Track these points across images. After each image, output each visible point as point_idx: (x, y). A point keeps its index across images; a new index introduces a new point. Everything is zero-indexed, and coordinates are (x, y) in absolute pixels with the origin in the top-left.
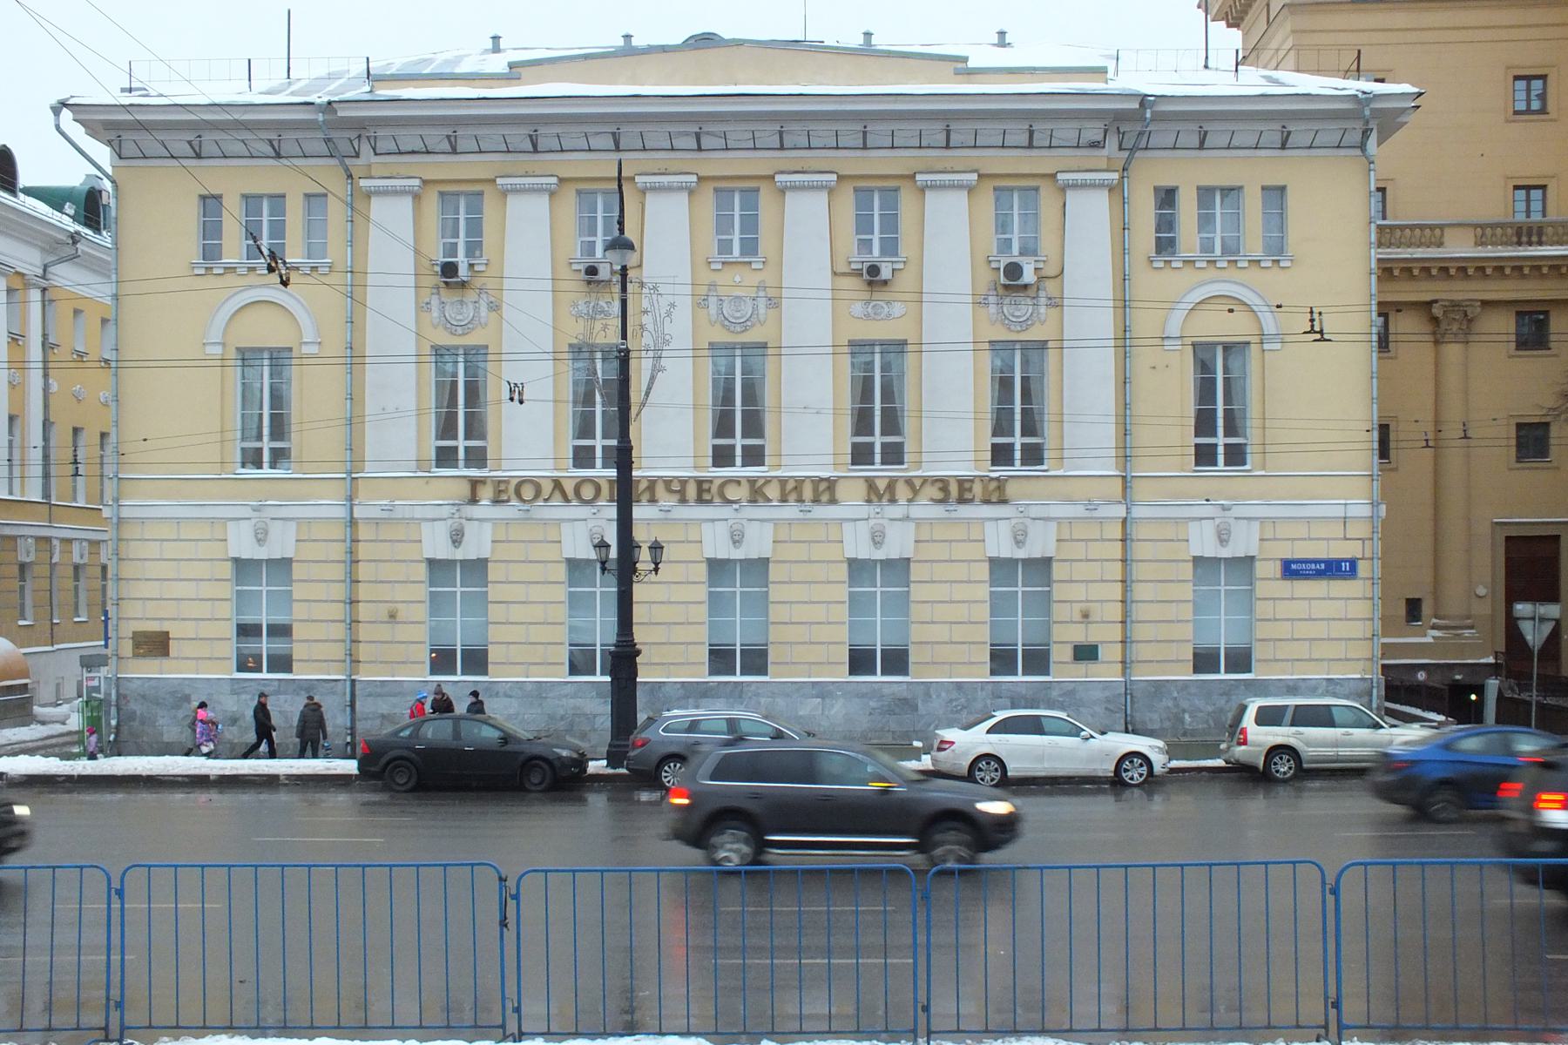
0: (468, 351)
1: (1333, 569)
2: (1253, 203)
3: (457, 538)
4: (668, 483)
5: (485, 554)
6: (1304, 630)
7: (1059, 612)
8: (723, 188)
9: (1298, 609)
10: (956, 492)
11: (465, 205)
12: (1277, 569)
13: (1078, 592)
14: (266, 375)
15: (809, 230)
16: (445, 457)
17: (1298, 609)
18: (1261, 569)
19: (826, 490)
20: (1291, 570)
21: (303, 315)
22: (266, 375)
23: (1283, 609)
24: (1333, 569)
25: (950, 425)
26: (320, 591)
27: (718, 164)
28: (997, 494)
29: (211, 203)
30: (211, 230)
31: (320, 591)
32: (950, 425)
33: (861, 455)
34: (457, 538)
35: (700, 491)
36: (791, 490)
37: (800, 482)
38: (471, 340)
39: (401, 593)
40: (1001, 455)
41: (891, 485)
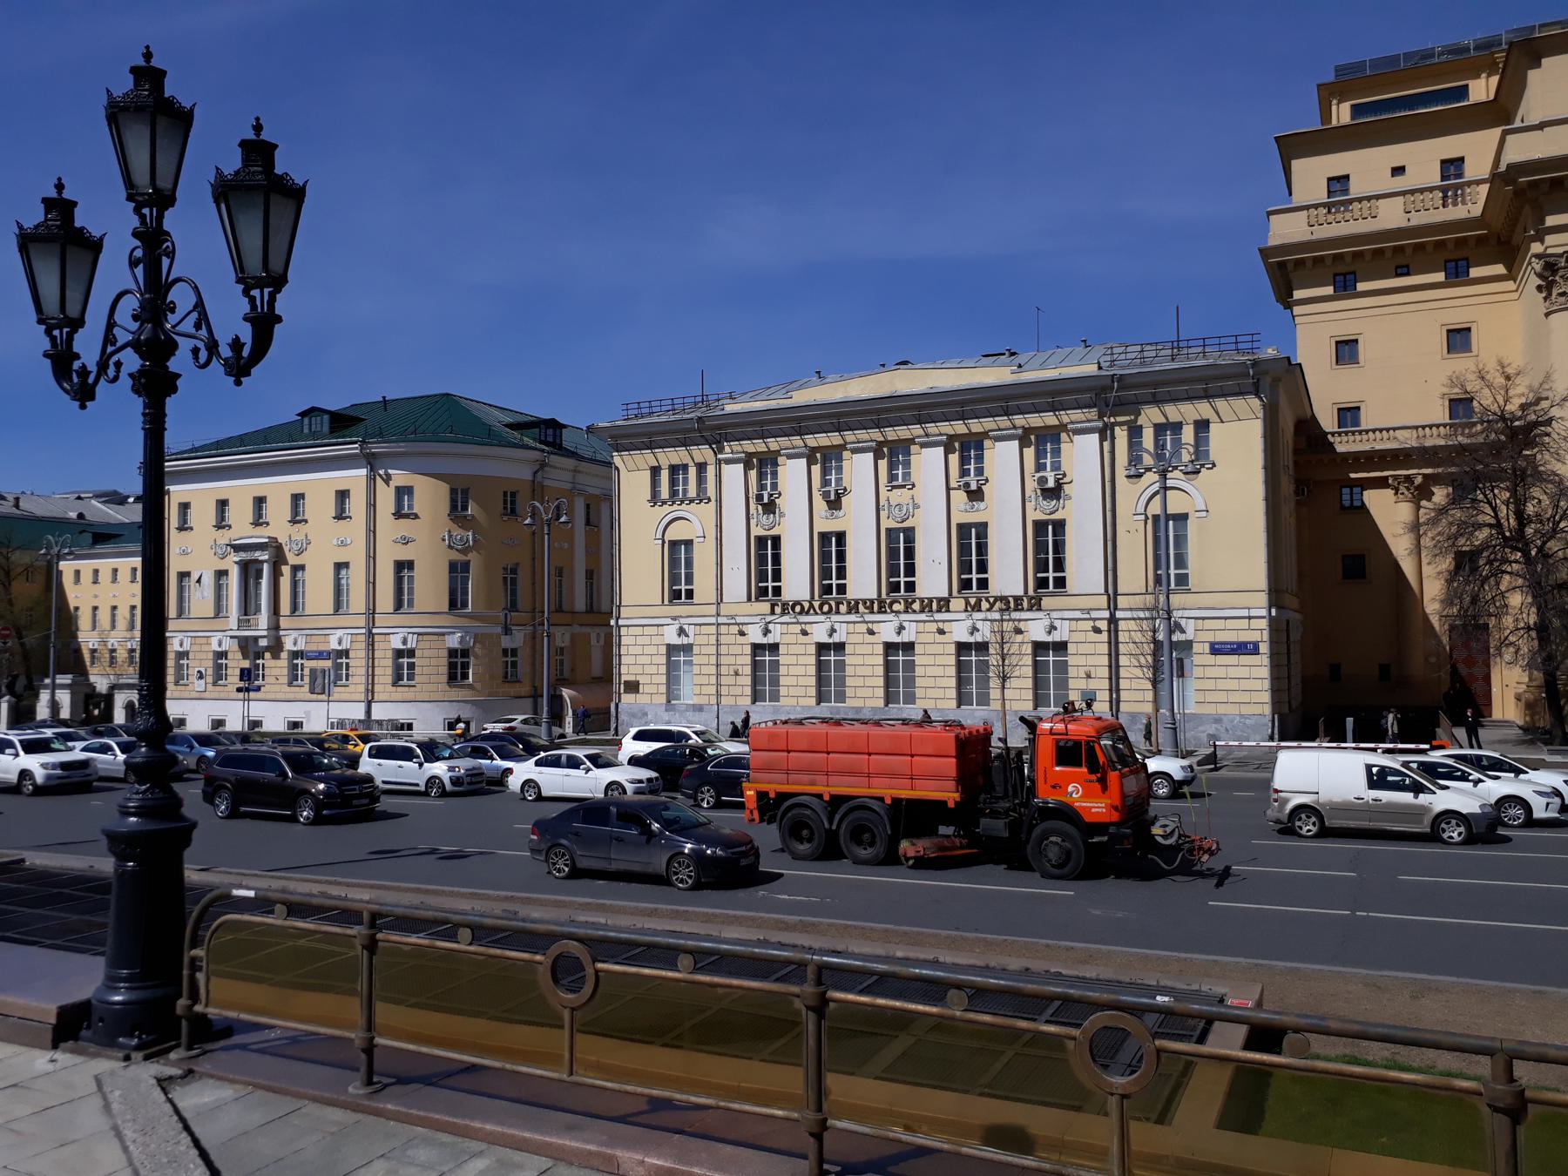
0: (977, 525)
1: (1241, 649)
2: (1188, 434)
3: (766, 632)
4: (864, 602)
5: (912, 639)
6: (1222, 684)
7: (1072, 672)
8: (811, 456)
9: (1221, 672)
10: (1010, 604)
11: (765, 464)
12: (1207, 648)
13: (1081, 660)
14: (678, 554)
15: (929, 465)
16: (763, 592)
17: (1221, 672)
18: (1196, 648)
19: (944, 605)
20: (1217, 649)
21: (695, 522)
22: (678, 554)
23: (1210, 672)
24: (1241, 649)
25: (1008, 570)
26: (705, 660)
27: (813, 441)
28: (1036, 605)
29: (655, 471)
30: (655, 483)
31: (705, 660)
32: (1008, 570)
33: (966, 585)
34: (766, 632)
35: (1016, 605)
36: (927, 605)
37: (931, 600)
38: (905, 525)
39: (1091, 660)
40: (1042, 583)
41: (979, 601)
